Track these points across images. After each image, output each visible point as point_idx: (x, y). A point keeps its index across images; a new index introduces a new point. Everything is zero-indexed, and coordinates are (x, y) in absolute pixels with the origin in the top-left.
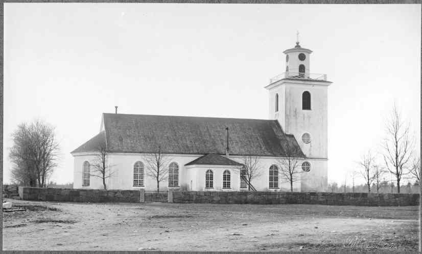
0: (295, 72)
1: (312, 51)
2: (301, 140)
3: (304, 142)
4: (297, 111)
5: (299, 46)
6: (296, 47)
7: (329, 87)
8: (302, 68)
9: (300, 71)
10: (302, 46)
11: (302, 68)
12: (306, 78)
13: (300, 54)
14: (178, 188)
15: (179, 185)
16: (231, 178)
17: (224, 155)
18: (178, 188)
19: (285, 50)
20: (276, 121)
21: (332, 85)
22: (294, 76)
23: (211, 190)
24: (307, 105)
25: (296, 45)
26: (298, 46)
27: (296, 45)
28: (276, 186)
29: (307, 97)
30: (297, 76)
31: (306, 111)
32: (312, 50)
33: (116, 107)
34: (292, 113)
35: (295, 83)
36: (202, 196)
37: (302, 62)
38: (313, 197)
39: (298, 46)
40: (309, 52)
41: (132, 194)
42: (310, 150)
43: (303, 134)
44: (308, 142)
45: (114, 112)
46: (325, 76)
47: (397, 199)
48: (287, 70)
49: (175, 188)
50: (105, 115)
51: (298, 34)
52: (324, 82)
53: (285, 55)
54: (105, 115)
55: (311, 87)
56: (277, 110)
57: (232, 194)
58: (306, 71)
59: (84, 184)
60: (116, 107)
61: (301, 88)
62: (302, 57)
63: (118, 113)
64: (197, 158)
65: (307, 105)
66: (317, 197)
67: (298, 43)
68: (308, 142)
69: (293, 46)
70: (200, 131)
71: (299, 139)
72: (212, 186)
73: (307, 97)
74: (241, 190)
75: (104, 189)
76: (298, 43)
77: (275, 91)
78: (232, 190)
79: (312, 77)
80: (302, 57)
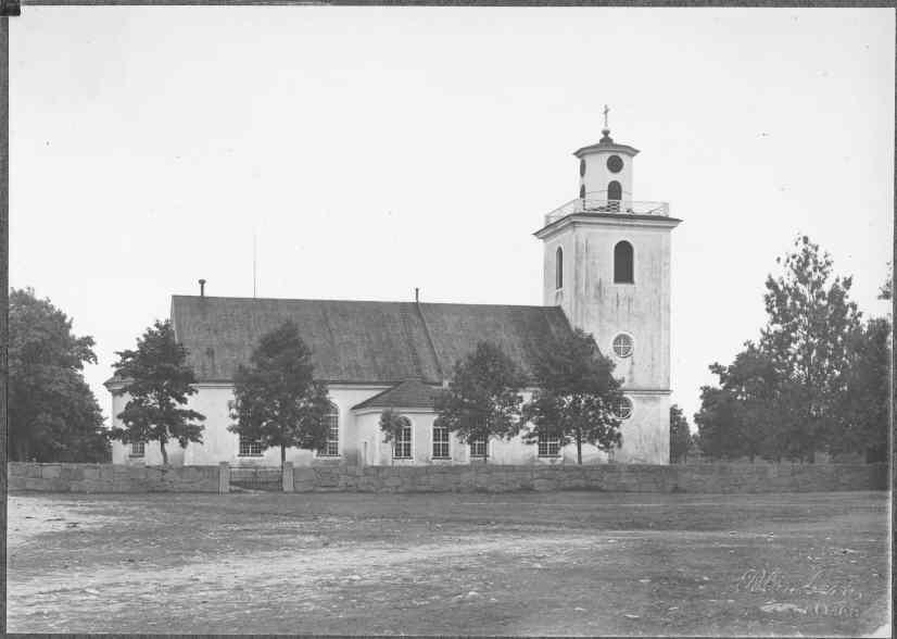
0: (599, 198)
1: (637, 151)
2: (612, 350)
3: (619, 354)
4: (603, 286)
5: (611, 140)
6: (602, 141)
7: (673, 231)
8: (615, 190)
9: (609, 197)
10: (617, 138)
11: (615, 190)
12: (623, 211)
13: (610, 159)
14: (338, 458)
15: (340, 452)
16: (413, 436)
17: (436, 384)
18: (338, 458)
19: (578, 149)
20: (558, 308)
21: (680, 225)
22: (596, 207)
23: (408, 462)
24: (624, 272)
25: (602, 136)
26: (606, 141)
27: (602, 136)
28: (446, 454)
29: (624, 252)
30: (602, 208)
31: (623, 288)
32: (637, 148)
33: (202, 282)
34: (592, 290)
35: (644, 226)
36: (358, 477)
37: (614, 179)
38: (609, 475)
39: (606, 141)
40: (632, 152)
41: (201, 474)
42: (631, 373)
43: (616, 335)
44: (627, 353)
45: (412, 299)
46: (666, 205)
47: (797, 477)
48: (583, 194)
49: (331, 458)
50: (175, 297)
51: (606, 112)
52: (664, 222)
53: (579, 161)
54: (175, 297)
55: (635, 232)
56: (561, 286)
57: (415, 472)
58: (623, 195)
59: (134, 452)
60: (202, 282)
61: (605, 240)
62: (615, 165)
63: (207, 294)
64: (378, 392)
65: (624, 272)
66: (616, 474)
67: (606, 133)
68: (627, 353)
69: (596, 139)
70: (388, 334)
71: (606, 348)
72: (408, 454)
73: (624, 252)
74: (243, 466)
75: (576, 460)
76: (606, 133)
77: (557, 240)
78: (453, 463)
79: (639, 210)
80: (615, 165)
